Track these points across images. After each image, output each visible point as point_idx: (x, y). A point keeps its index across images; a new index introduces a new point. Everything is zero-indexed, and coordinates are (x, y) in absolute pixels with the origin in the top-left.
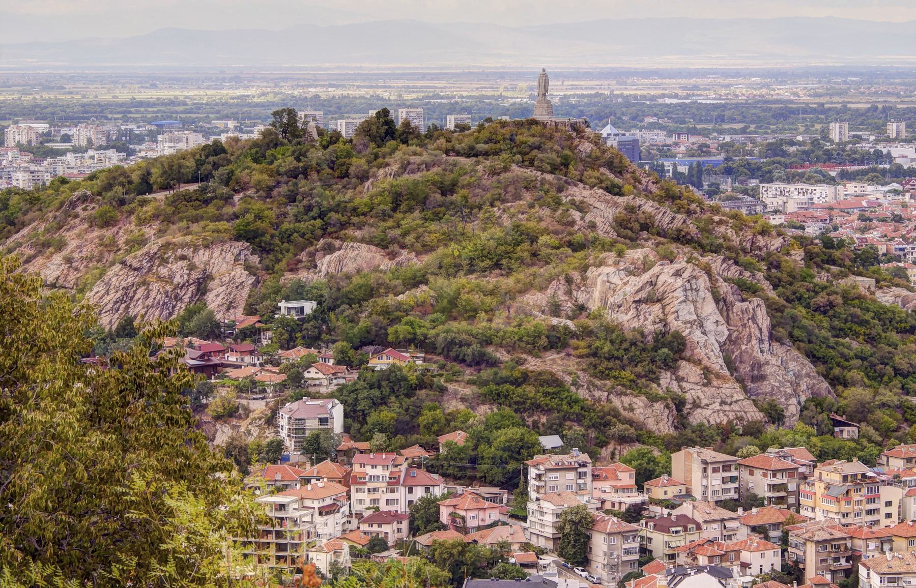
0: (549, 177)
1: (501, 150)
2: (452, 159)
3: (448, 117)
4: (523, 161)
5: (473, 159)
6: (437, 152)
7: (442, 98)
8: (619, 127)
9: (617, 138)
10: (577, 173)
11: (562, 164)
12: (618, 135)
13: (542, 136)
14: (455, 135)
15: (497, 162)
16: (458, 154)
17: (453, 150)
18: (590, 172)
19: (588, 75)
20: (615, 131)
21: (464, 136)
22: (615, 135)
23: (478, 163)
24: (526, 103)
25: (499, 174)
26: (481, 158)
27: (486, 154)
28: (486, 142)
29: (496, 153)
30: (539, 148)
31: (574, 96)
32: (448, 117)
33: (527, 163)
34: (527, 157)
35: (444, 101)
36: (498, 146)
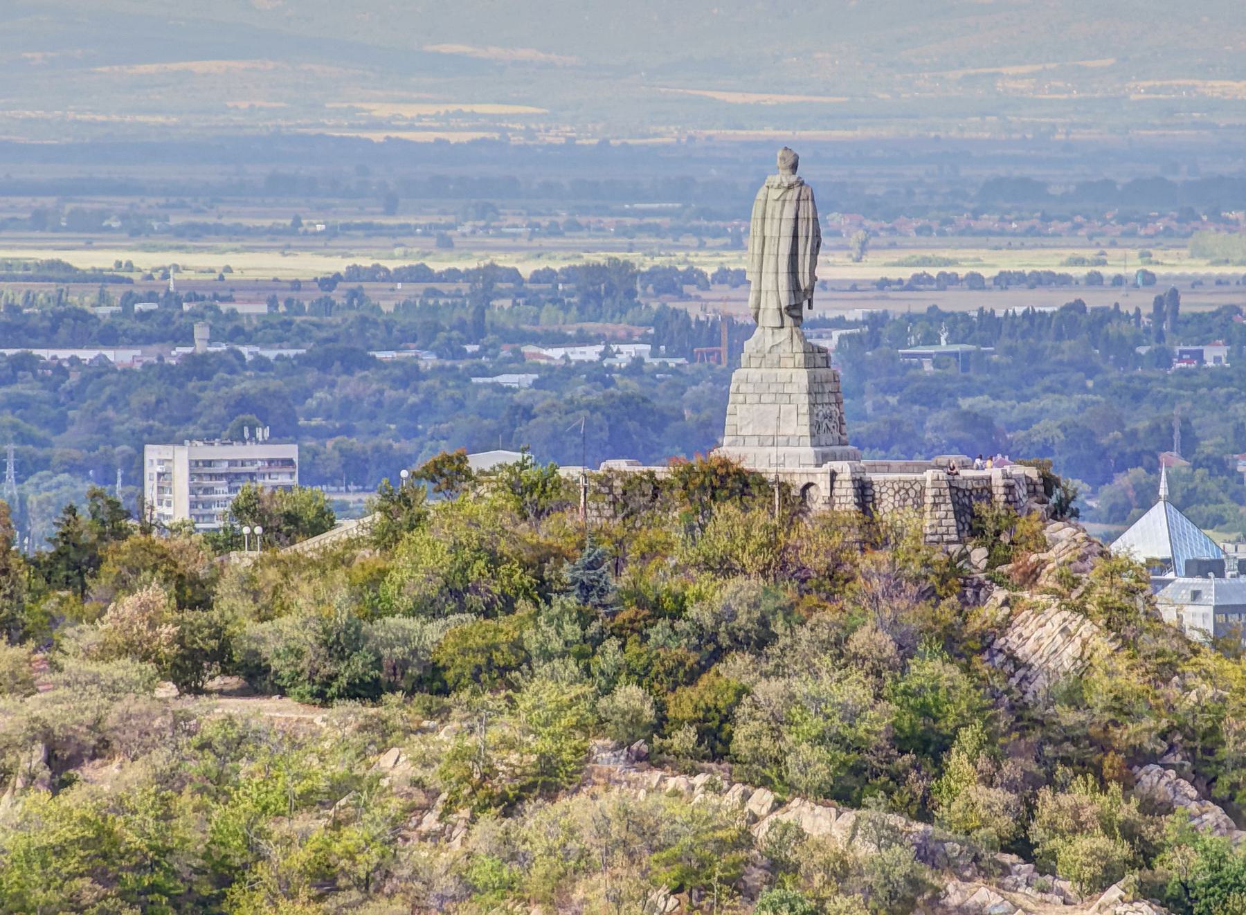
0: (823, 824)
1: (523, 659)
2: (221, 710)
3: (153, 454)
4: (661, 725)
5: (353, 712)
6: (124, 669)
7: (110, 337)
8: (1216, 522)
9: (1209, 585)
10: (998, 796)
11: (901, 742)
12: (1214, 568)
13: (780, 565)
14: (242, 560)
15: (509, 732)
16: (257, 679)
17: (222, 655)
18: (1080, 794)
19: (1014, 196)
20: (1200, 545)
21: (290, 568)
22: (1200, 568)
23: (382, 735)
24: (636, 367)
25: (510, 806)
26: (393, 708)
27: (431, 682)
28: (427, 609)
29: (502, 671)
30: (759, 641)
31: (256, 289)
32: (153, 454)
33: (684, 738)
34: (684, 703)
35: (120, 356)
36: (506, 627)
